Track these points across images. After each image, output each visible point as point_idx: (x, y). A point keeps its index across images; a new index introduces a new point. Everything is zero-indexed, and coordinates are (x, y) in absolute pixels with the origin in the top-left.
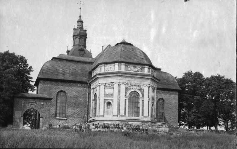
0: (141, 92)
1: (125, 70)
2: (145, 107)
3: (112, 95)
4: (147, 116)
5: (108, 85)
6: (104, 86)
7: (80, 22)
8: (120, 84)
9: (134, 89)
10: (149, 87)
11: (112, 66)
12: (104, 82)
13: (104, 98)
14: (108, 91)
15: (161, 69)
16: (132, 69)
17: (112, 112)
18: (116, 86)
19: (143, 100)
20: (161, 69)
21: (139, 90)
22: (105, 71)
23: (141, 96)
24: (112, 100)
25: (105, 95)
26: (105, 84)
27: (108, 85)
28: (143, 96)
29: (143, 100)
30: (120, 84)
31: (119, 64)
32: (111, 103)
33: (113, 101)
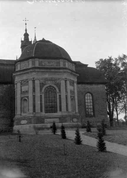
0: (57, 86)
1: (39, 65)
2: (65, 103)
3: (27, 92)
4: (66, 111)
5: (24, 82)
6: (20, 83)
7: (26, 30)
8: (35, 80)
9: (49, 83)
10: (66, 81)
11: (26, 62)
12: (20, 80)
13: (21, 96)
14: (24, 88)
15: (88, 65)
16: (46, 63)
17: (74, 109)
18: (30, 83)
19: (60, 94)
20: (88, 65)
21: (55, 84)
22: (20, 68)
23: (57, 90)
24: (28, 97)
25: (22, 93)
26: (20, 81)
27: (24, 82)
28: (60, 90)
29: (35, 95)
30: (35, 80)
31: (33, 60)
32: (27, 100)
33: (28, 98)
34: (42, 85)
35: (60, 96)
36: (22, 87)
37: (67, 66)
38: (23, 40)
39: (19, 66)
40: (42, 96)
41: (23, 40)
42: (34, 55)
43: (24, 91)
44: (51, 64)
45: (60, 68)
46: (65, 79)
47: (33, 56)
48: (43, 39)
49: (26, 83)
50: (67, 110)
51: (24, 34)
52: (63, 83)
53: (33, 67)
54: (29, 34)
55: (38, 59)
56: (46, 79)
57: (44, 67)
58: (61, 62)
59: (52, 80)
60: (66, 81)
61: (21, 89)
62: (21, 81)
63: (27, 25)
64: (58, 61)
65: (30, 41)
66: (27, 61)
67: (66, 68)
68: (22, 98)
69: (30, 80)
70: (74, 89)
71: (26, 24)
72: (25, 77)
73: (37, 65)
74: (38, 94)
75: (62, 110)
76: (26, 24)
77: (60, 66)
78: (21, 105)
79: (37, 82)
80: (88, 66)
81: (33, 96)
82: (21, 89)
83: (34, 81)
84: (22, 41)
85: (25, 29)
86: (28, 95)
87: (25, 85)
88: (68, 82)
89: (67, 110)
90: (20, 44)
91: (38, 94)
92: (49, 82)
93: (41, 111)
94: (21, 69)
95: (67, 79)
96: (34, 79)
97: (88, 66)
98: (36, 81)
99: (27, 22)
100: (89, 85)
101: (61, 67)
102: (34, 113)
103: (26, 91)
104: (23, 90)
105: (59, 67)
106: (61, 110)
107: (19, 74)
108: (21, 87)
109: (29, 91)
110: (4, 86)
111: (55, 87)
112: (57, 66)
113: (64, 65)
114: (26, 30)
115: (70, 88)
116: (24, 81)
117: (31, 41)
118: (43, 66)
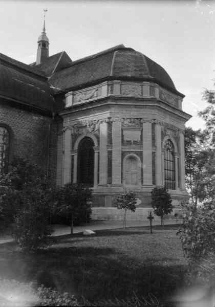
8: (112, 122)
13: (122, 149)
18: (147, 127)
19: (154, 151)
21: (174, 138)
24: (140, 154)
28: (99, 144)
29: (155, 152)
37: (157, 96)
42: (114, 73)
43: (128, 139)
45: (142, 100)
46: (153, 121)
47: (111, 75)
50: (110, 182)
60: (154, 125)
61: (123, 136)
66: (139, 84)
68: (123, 154)
69: (102, 122)
73: (116, 93)
79: (158, 128)
82: (123, 136)
96: (111, 120)
98: (144, 124)
102: (109, 185)
103: (135, 142)
107: (151, 104)
110: (34, 117)
116: (132, 120)
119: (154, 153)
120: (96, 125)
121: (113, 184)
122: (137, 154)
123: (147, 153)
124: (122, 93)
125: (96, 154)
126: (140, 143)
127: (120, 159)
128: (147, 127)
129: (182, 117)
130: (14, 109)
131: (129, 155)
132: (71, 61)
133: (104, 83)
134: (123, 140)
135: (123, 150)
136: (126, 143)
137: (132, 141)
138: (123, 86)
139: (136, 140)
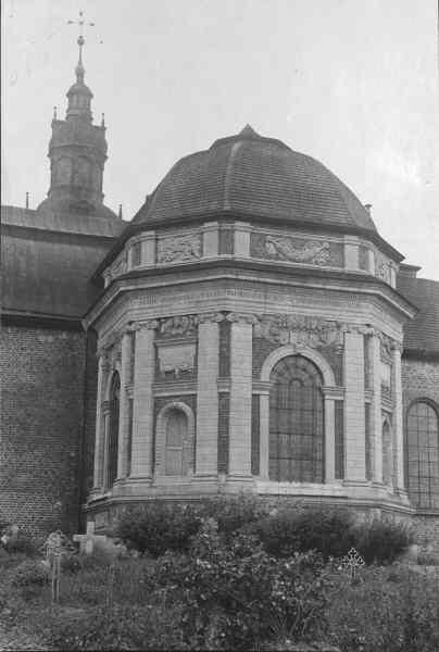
0: (329, 360)
1: (253, 253)
4: (364, 478)
6: (152, 333)
7: (80, 73)
10: (367, 337)
11: (189, 236)
12: (151, 314)
13: (154, 392)
14: (174, 357)
15: (418, 269)
18: (209, 333)
19: (368, 401)
21: (319, 349)
22: (156, 261)
24: (192, 400)
25: (162, 377)
26: (156, 323)
28: (340, 379)
33: (194, 408)
34: (261, 347)
35: (340, 405)
36: (162, 351)
38: (62, 117)
39: (147, 249)
40: (262, 398)
41: (62, 117)
43: (169, 368)
44: (307, 253)
46: (367, 331)
48: (248, 129)
49: (180, 331)
50: (223, 467)
51: (67, 91)
52: (353, 346)
53: (226, 261)
54: (93, 91)
55: (248, 225)
56: (282, 323)
57: (272, 262)
58: (237, 235)
59: (309, 330)
60: (367, 337)
61: (157, 359)
62: (159, 319)
63: (83, 47)
64: (336, 240)
65: (97, 127)
67: (370, 280)
68: (158, 403)
70: (392, 378)
71: (81, 43)
72: (180, 306)
73: (242, 252)
74: (242, 387)
75: (350, 474)
76: (81, 43)
77: (343, 266)
78: (154, 432)
79: (241, 335)
80: (419, 275)
81: (221, 395)
82: (157, 359)
83: (225, 327)
84: (55, 123)
85: (76, 64)
86: (194, 392)
87: (176, 340)
88: (375, 343)
89: (369, 475)
90: (48, 134)
91: (242, 387)
92: (294, 337)
93: (255, 470)
94: (159, 265)
95: (230, 317)
97: (419, 275)
98: (235, 328)
99: (86, 32)
100: (427, 366)
101: (347, 269)
102: (223, 477)
103: (184, 372)
104: (164, 367)
105: (340, 269)
106: (340, 473)
108: (156, 347)
109: (200, 372)
110: (42, 339)
111: (319, 360)
112: (328, 263)
113: (364, 264)
114: (80, 73)
115: (381, 373)
117: (99, 124)
118: (270, 257)
119: (367, 405)
120: (366, 333)
121: (345, 479)
122: (185, 402)
123: (207, 395)
124: (159, 259)
125: (330, 407)
126: (189, 375)
127: (150, 412)
128: (209, 333)
129: (162, 287)
130: (46, 332)
131: (169, 405)
132: (360, 204)
133: (148, 233)
134: (157, 368)
135: (158, 395)
136: (164, 376)
137: (177, 370)
138: (160, 242)
139: (185, 367)
